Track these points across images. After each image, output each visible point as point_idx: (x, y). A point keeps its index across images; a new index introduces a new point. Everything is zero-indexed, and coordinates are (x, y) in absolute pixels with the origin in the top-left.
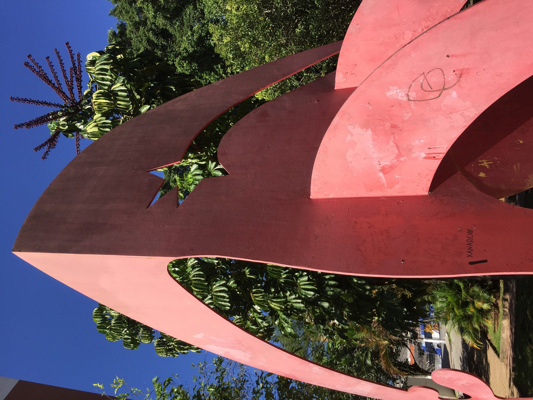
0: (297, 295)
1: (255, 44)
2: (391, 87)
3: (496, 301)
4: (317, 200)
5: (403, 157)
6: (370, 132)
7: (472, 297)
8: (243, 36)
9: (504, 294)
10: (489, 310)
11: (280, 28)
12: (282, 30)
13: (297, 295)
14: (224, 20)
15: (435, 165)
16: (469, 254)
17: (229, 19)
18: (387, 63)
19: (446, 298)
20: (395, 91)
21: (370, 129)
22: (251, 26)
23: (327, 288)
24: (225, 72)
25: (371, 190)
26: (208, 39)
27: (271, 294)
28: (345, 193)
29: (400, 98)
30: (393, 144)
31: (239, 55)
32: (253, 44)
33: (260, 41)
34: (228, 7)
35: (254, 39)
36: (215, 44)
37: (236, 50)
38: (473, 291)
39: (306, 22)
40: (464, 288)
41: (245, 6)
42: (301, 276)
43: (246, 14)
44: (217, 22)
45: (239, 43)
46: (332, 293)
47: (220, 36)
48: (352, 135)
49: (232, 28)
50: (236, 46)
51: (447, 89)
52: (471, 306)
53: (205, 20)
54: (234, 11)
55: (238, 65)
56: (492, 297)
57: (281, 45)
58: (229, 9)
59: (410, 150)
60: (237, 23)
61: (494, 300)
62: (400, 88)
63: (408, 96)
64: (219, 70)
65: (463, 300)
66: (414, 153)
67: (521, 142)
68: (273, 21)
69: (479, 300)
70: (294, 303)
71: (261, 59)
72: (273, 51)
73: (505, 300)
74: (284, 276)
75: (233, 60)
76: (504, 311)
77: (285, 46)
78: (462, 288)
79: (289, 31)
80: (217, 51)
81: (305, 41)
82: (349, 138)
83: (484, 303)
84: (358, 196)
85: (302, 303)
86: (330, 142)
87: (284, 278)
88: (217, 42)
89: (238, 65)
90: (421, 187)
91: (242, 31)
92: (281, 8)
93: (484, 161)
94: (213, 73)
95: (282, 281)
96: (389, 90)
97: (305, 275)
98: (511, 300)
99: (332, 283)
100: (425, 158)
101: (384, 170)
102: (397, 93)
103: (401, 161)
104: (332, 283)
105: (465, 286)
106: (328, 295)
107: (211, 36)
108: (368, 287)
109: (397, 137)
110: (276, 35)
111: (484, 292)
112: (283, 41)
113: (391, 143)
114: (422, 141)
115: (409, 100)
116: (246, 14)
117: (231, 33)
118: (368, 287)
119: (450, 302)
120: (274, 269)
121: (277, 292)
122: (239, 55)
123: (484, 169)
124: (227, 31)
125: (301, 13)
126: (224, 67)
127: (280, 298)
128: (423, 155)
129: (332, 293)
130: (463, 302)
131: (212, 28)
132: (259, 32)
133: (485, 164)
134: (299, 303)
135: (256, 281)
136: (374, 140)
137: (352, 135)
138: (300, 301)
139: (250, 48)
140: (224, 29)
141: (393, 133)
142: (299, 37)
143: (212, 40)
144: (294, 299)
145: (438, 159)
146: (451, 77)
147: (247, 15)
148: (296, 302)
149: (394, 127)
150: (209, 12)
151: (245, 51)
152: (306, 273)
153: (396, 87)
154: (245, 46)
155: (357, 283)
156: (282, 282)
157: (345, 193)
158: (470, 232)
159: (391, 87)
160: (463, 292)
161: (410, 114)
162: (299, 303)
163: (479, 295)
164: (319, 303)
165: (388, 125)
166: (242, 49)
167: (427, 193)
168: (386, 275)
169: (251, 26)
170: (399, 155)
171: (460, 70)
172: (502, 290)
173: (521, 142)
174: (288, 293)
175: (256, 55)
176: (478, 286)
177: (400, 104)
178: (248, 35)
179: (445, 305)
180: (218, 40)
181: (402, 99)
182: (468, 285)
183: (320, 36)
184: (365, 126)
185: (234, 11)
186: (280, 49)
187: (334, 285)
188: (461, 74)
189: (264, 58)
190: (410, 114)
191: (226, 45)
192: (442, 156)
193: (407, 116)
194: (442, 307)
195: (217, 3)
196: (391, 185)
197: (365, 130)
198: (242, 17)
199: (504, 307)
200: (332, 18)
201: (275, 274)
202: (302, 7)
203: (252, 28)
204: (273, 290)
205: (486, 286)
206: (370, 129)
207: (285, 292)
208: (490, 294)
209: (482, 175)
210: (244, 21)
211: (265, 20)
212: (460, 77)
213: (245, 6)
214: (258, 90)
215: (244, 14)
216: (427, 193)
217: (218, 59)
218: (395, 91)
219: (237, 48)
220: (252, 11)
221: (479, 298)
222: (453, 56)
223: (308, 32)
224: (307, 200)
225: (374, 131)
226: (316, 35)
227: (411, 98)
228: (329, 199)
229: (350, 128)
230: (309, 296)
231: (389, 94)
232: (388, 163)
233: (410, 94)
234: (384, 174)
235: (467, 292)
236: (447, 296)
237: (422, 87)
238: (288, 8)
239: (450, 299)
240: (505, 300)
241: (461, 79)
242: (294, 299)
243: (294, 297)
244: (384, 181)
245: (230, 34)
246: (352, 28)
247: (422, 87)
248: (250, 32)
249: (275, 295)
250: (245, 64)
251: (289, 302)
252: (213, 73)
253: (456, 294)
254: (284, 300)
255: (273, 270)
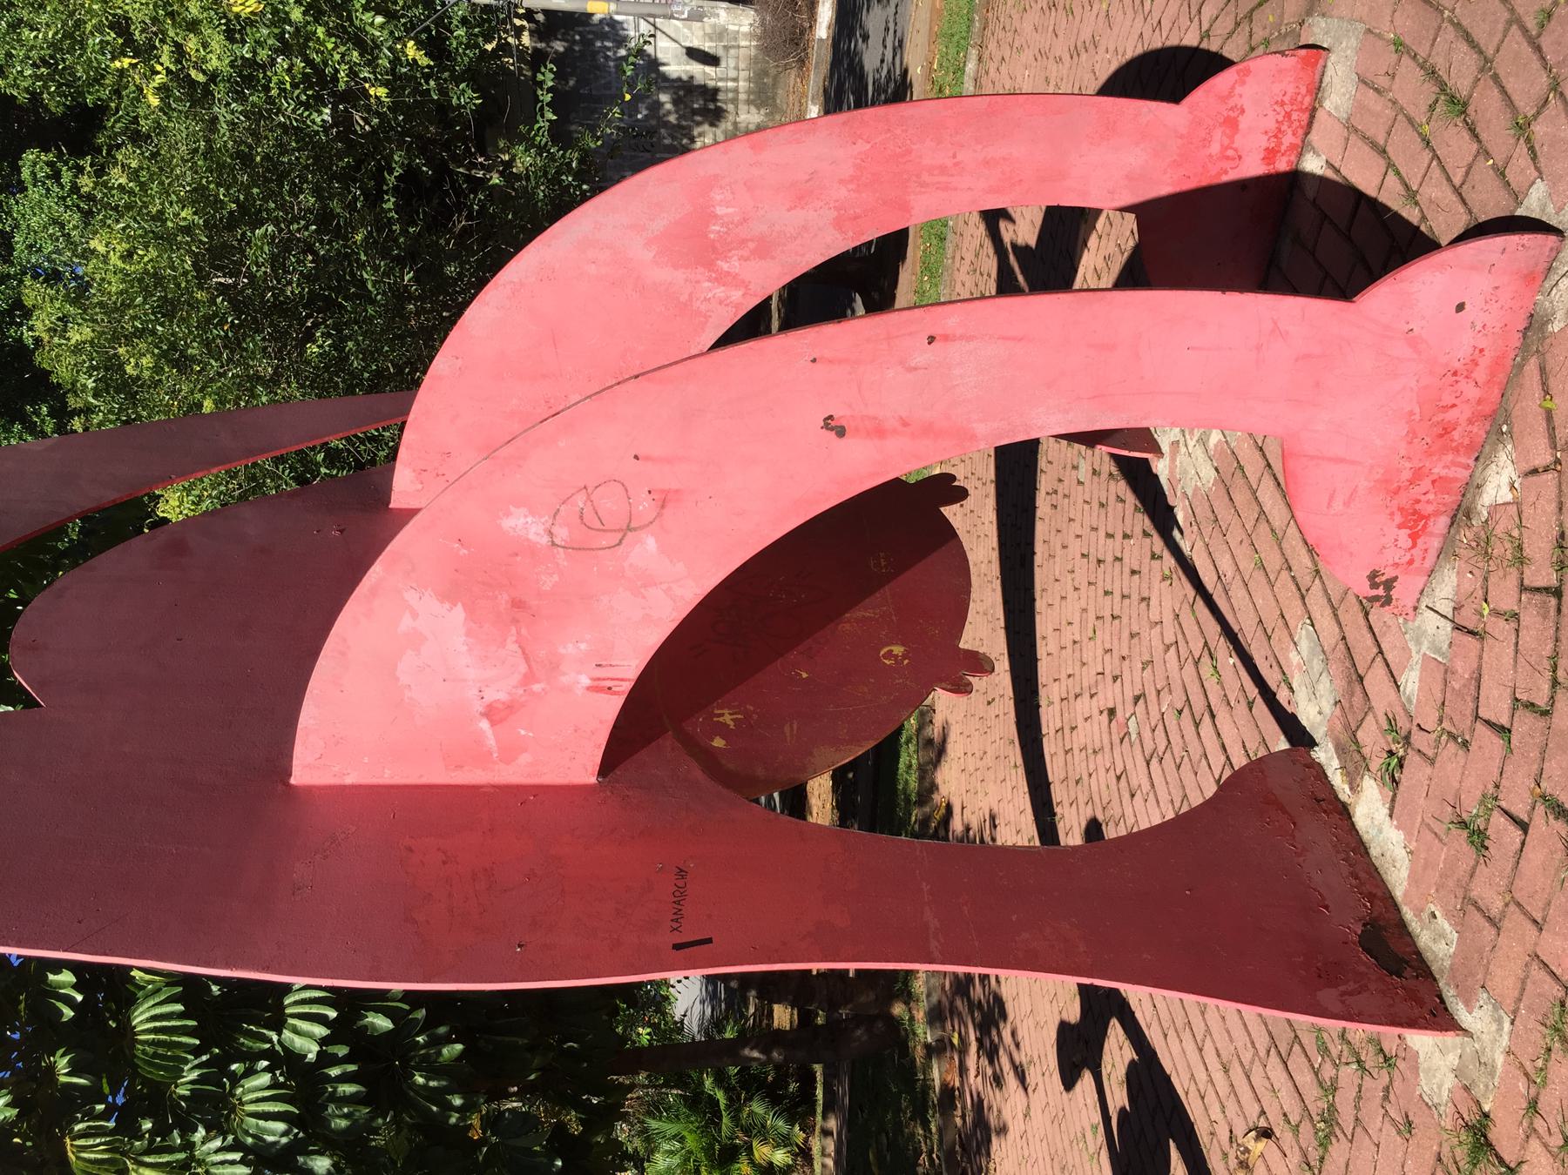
0: (230, 1138)
1: (175, 364)
2: (512, 509)
3: (806, 1141)
4: (309, 789)
5: (538, 682)
6: (459, 613)
7: (747, 1131)
8: (139, 334)
9: (825, 1118)
10: (789, 1166)
11: (257, 331)
12: (264, 339)
13: (230, 1138)
14: (76, 278)
15: (610, 708)
16: (675, 925)
17: (98, 277)
18: (506, 451)
19: (682, 1140)
20: (522, 520)
21: (459, 607)
22: (168, 309)
23: (331, 1108)
24: (61, 429)
25: (459, 767)
26: (13, 323)
27: (141, 1138)
28: (387, 773)
29: (532, 537)
30: (515, 647)
31: (113, 380)
32: (169, 361)
33: (194, 356)
34: (97, 244)
35: (173, 347)
36: (38, 340)
37: (107, 369)
38: (751, 1113)
39: (339, 331)
40: (728, 1107)
41: (153, 253)
42: (250, 1072)
43: (155, 274)
44: (53, 277)
45: (121, 351)
46: (343, 1123)
47: (59, 319)
48: (415, 615)
49: (101, 304)
50: (110, 359)
51: (635, 529)
52: (743, 1158)
53: (12, 264)
54: (114, 259)
55: (110, 411)
56: (797, 1128)
57: (258, 379)
58: (101, 249)
59: (554, 666)
60: (121, 293)
61: (799, 1135)
62: (532, 513)
63: (551, 533)
64: (43, 421)
65: (725, 1141)
66: (564, 674)
67: (805, 675)
68: (236, 307)
69: (765, 1141)
70: (214, 1164)
71: (190, 408)
72: (230, 391)
73: (826, 1133)
74: (194, 1075)
75: (95, 396)
76: (824, 1166)
77: (272, 383)
78: (722, 1107)
79: (288, 343)
80: (42, 360)
81: (331, 378)
82: (406, 623)
83: (777, 1146)
84: (425, 780)
85: (243, 1162)
86: (357, 630)
87: (192, 1082)
88: (45, 337)
89: (110, 411)
90: (578, 763)
91: (134, 318)
92: (265, 281)
93: (726, 711)
94: (17, 427)
95: (182, 1091)
96: (508, 514)
97: (265, 1070)
98: (839, 1134)
99: (348, 1089)
100: (588, 688)
101: (490, 713)
102: (525, 525)
103: (533, 693)
104: (348, 1089)
105: (730, 1099)
106: (332, 1131)
107: (27, 313)
108: (457, 1101)
109: (524, 631)
110: (246, 350)
111: (778, 1115)
112: (265, 368)
113: (512, 646)
114: (583, 646)
115: (553, 544)
116: (155, 274)
117: (99, 318)
118: (457, 1101)
119: (690, 1152)
120: (160, 1051)
121: (161, 1130)
122: (113, 380)
123: (722, 730)
124: (85, 311)
125: (321, 304)
126: (62, 414)
127: (171, 1150)
128: (585, 681)
129: (343, 1123)
130: (723, 1149)
131: (32, 292)
132: (191, 332)
133: (727, 718)
134: (233, 1163)
135: (93, 1094)
136: (469, 633)
137: (415, 615)
138: (237, 1156)
139: (157, 369)
140: (74, 302)
141: (515, 621)
142: (316, 368)
143: (31, 329)
144: (218, 1151)
145: (615, 693)
146: (644, 506)
147: (159, 279)
148: (222, 1163)
149: (517, 604)
150: (31, 246)
151: (138, 378)
152: (265, 1063)
153: (523, 510)
154: (139, 363)
155: (425, 1087)
156: (183, 1097)
157: (387, 773)
158: (682, 873)
159: (512, 509)
160: (725, 1120)
161: (556, 578)
162: (233, 1163)
163: (764, 1126)
164: (301, 1159)
165: (504, 598)
166: (129, 369)
167: (593, 780)
168: (474, 982)
169: (168, 309)
170: (529, 678)
171: (662, 491)
172: (819, 1110)
173: (805, 675)
174: (201, 1132)
175: (174, 393)
176: (762, 1099)
177: (531, 549)
178: (153, 332)
179: (676, 1160)
180: (52, 331)
181: (537, 539)
182: (739, 1099)
183: (378, 374)
184: (449, 595)
185: (114, 259)
186: (252, 390)
187: (353, 1095)
188: (664, 499)
189: (200, 406)
190: (556, 578)
191: (77, 349)
192: (627, 687)
193: (548, 582)
194: (669, 1168)
195: (62, 226)
196: (509, 753)
197: (447, 606)
198: (140, 281)
199: (824, 1154)
200: (412, 334)
201: (161, 1067)
202: (330, 288)
203: (170, 316)
204: (147, 1125)
205: (784, 1097)
206: (459, 607)
207: (187, 1129)
208: (791, 1121)
209: (718, 743)
210: (148, 294)
211: (213, 301)
212: (663, 507)
213: (153, 253)
214: (166, 481)
215: (146, 272)
216: (593, 780)
217: (43, 387)
218: (522, 520)
219: (113, 365)
220: (174, 269)
221: (763, 1133)
222: (647, 458)
223: (344, 359)
224: (280, 787)
225: (470, 611)
226: (364, 369)
227: (558, 541)
228: (343, 788)
229: (411, 597)
230: (270, 1139)
231: (508, 523)
232: (502, 696)
233: (555, 530)
234: (493, 724)
235: (736, 1119)
236: (685, 1133)
237: (581, 518)
238: (290, 283)
239: (691, 1142)
240: (826, 1133)
241: (665, 511)
242: (218, 1151)
243: (218, 1143)
244: (491, 742)
245: (94, 321)
246: (443, 363)
247: (581, 518)
248: (162, 325)
249: (152, 1141)
250: (136, 412)
251: (200, 1163)
252: (17, 427)
253: (706, 1126)
254: (182, 1156)
255: (155, 1055)
